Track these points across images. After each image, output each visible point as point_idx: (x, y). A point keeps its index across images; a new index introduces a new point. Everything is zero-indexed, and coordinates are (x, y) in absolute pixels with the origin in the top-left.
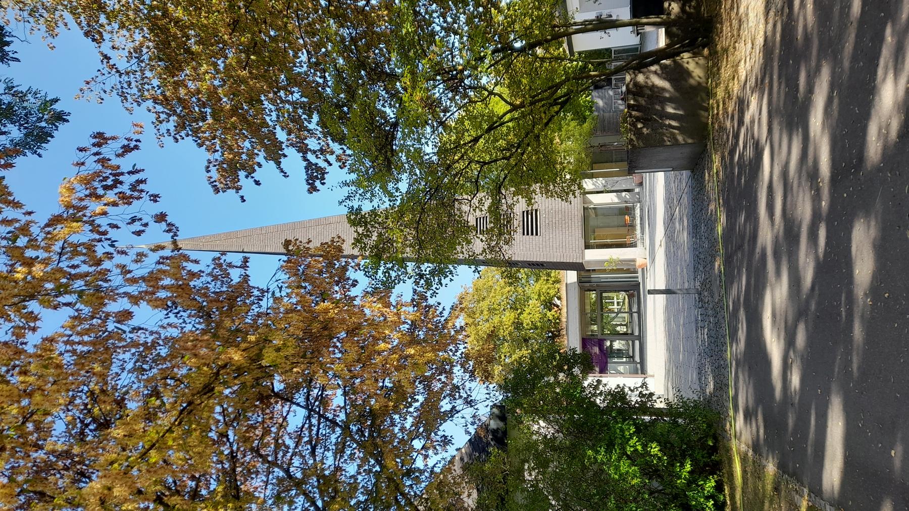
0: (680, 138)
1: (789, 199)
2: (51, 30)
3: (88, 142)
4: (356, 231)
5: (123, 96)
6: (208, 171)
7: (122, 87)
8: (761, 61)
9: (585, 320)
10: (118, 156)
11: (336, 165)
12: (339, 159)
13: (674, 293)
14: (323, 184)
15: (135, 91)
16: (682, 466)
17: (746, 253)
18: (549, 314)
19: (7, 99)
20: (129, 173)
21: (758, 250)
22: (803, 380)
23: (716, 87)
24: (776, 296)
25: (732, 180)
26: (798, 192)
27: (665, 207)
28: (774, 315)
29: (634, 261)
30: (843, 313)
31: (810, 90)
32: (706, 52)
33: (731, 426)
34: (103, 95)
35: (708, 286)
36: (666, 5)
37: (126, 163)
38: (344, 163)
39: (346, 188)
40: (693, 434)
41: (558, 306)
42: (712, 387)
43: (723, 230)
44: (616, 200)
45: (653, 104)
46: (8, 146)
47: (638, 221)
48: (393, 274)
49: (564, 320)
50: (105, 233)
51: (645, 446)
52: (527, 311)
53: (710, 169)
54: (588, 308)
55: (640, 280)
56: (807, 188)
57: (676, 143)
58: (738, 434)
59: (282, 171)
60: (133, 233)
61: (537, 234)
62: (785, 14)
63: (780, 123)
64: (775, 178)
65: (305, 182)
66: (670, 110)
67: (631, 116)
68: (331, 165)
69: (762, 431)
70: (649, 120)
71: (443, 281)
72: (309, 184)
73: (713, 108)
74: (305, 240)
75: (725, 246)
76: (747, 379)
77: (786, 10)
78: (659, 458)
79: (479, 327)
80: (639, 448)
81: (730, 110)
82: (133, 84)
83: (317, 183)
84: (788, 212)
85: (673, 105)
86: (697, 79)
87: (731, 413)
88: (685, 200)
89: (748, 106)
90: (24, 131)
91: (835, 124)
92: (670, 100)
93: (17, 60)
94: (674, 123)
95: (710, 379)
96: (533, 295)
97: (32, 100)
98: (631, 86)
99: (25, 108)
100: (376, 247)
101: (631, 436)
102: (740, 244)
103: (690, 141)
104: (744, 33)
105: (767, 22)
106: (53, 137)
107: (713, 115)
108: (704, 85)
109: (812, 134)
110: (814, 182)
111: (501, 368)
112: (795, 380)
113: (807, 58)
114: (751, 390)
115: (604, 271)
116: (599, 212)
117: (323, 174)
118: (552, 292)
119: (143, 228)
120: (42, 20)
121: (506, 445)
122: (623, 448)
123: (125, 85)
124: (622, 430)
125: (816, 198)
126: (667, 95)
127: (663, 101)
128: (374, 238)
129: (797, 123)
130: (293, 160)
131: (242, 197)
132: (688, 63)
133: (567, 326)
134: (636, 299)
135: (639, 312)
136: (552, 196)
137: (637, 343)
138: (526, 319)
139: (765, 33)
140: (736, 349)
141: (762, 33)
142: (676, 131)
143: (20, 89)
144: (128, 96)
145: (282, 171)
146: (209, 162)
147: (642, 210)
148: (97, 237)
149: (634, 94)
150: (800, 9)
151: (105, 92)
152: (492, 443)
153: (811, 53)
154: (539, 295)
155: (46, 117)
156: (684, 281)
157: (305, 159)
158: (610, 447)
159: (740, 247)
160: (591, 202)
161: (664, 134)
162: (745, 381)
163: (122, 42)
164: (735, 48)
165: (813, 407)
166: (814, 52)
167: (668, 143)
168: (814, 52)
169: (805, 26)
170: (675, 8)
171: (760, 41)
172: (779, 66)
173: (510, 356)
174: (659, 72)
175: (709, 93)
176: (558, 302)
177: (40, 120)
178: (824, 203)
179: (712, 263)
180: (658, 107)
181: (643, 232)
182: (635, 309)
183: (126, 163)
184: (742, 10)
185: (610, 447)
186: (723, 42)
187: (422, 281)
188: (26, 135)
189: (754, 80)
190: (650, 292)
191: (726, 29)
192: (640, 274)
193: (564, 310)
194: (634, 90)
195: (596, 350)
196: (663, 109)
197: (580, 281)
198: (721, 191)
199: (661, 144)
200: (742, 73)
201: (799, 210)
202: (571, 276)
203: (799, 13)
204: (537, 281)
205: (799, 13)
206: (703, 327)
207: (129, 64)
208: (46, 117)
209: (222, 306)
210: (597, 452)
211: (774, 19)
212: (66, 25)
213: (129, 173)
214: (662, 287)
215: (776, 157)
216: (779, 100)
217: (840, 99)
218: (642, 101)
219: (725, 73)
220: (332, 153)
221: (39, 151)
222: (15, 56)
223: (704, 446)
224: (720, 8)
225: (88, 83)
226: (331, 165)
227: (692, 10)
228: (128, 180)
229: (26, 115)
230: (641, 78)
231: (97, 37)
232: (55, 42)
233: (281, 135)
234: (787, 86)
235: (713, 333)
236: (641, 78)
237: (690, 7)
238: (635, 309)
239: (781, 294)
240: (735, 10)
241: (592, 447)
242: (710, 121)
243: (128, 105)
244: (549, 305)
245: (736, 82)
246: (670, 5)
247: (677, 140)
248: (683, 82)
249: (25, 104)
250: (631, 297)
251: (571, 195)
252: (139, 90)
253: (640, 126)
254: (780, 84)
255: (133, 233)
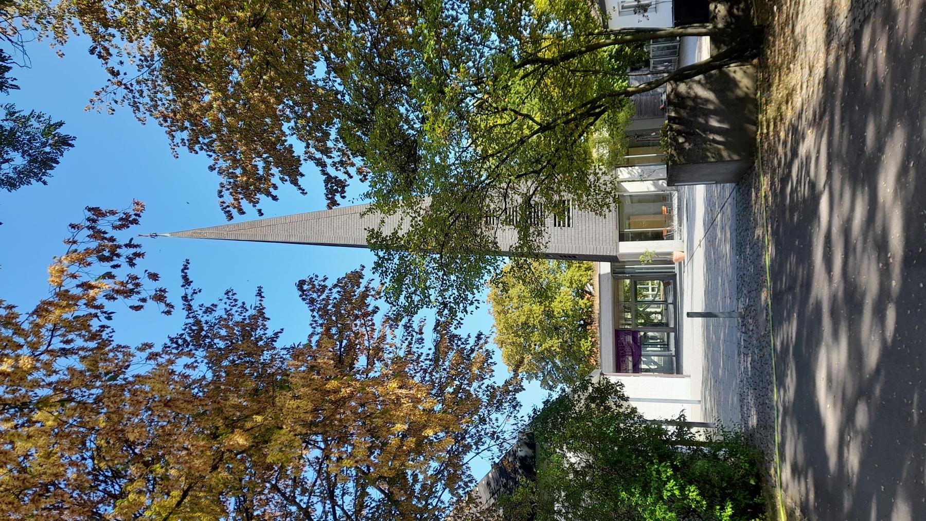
0: (725, 154)
1: (851, 259)
2: (60, 36)
3: (81, 217)
4: (377, 255)
5: (135, 106)
6: (221, 196)
7: (134, 97)
8: (821, 94)
9: (619, 308)
10: (115, 228)
11: (356, 177)
12: (359, 172)
13: (716, 316)
14: (344, 197)
15: (147, 100)
16: (723, 509)
17: (798, 298)
18: (581, 302)
19: (8, 125)
20: (126, 246)
21: (812, 300)
22: (863, 463)
23: (766, 104)
24: (831, 360)
25: (784, 212)
26: (862, 257)
27: (706, 208)
28: (829, 379)
29: (670, 254)
30: (915, 416)
31: (880, 148)
32: (755, 61)
33: (776, 472)
34: (114, 105)
35: (753, 314)
36: (712, 7)
37: (122, 237)
38: (365, 176)
39: (368, 201)
40: (731, 474)
41: (590, 293)
42: (755, 421)
43: (772, 261)
44: (652, 188)
45: (696, 116)
46: (11, 175)
47: (675, 212)
48: (416, 298)
49: (596, 307)
50: (100, 307)
51: (682, 489)
52: (559, 299)
53: (758, 190)
54: (622, 298)
55: (677, 271)
56: (874, 257)
57: (720, 159)
58: (784, 485)
59: (300, 189)
60: (131, 307)
61: (569, 226)
62: (850, 51)
63: (842, 172)
64: (835, 230)
65: (324, 197)
66: (714, 123)
67: (671, 129)
68: (351, 177)
69: (812, 496)
70: (692, 135)
71: (469, 309)
72: (328, 199)
73: (762, 126)
74: (321, 278)
75: (776, 276)
76: (796, 433)
77: (852, 48)
78: (698, 502)
79: (509, 315)
80: (677, 492)
81: (782, 134)
82: (145, 94)
83: (338, 197)
84: (850, 274)
85: (718, 118)
86: (745, 89)
87: (777, 458)
88: (728, 210)
89: (804, 138)
90: (27, 158)
91: (910, 199)
92: (715, 112)
93: (17, 87)
94: (718, 138)
95: (753, 412)
96: (564, 283)
97: (36, 125)
98: (672, 97)
99: (28, 133)
100: (398, 270)
101: (669, 479)
102: (792, 289)
103: (736, 157)
104: (801, 56)
105: (828, 53)
106: (57, 163)
107: (762, 133)
108: (752, 96)
109: (881, 199)
110: (883, 254)
111: (530, 357)
112: (853, 460)
113: (878, 113)
114: (800, 448)
115: (639, 262)
116: (635, 199)
117: (343, 187)
118: (584, 280)
119: (141, 304)
120: (50, 27)
121: (535, 474)
122: (660, 492)
123: (137, 95)
124: (658, 472)
125: (885, 273)
126: (711, 107)
127: (707, 114)
128: (396, 261)
129: (863, 180)
130: (311, 175)
131: (260, 211)
132: (735, 72)
133: (600, 318)
134: (671, 287)
135: (674, 303)
136: (585, 207)
137: (672, 335)
138: (556, 306)
139: (826, 64)
140: (783, 396)
141: (822, 62)
142: (721, 147)
143: (22, 114)
144: (141, 106)
145: (300, 189)
146: (222, 186)
147: (679, 199)
148: (93, 311)
149: (675, 105)
150: (869, 51)
151: (116, 102)
152: (520, 471)
153: (882, 107)
154: (571, 283)
155: (50, 142)
156: (725, 302)
157: (324, 172)
158: (645, 492)
159: (791, 288)
160: (626, 191)
161: (708, 150)
162: (793, 433)
163: (133, 53)
164: (789, 69)
165: (874, 497)
166: (886, 106)
167: (713, 160)
168: (886, 106)
169: (875, 74)
170: (721, 9)
171: (819, 71)
172: (842, 108)
173: (541, 345)
174: (703, 81)
175: (757, 107)
176: (591, 288)
177: (44, 145)
178: (894, 283)
179: (759, 292)
180: (701, 120)
181: (680, 224)
182: (670, 300)
183: (122, 237)
184: (798, 29)
185: (645, 492)
186: (775, 55)
187: (446, 311)
188: (29, 162)
189: (811, 112)
190: (689, 315)
191: (779, 43)
192: (676, 265)
193: (597, 302)
194: (676, 101)
195: (630, 339)
196: (707, 122)
197: (614, 272)
198: (771, 218)
199: (704, 159)
200: (798, 100)
201: (863, 278)
202: (605, 268)
203: (867, 56)
204: (569, 267)
205: (867, 56)
206: (746, 355)
207: (140, 73)
208: (50, 142)
209: (238, 341)
210: (633, 495)
211: (837, 52)
212: (75, 30)
213: (126, 246)
214: (700, 308)
215: (835, 207)
216: (841, 143)
217: (917, 172)
218: (684, 113)
219: (778, 93)
220: (353, 165)
221: (44, 178)
222: (14, 83)
223: (746, 485)
224: (773, 20)
225: (98, 94)
226: (351, 177)
227: (740, 13)
228: (126, 252)
229: (29, 141)
230: (682, 88)
231: (104, 53)
232: (64, 49)
233: (299, 148)
234: (851, 132)
235: (758, 366)
236: (682, 88)
237: (738, 10)
238: (670, 300)
239: (839, 359)
240: (790, 27)
241: (627, 490)
242: (758, 137)
243: (140, 115)
244: (581, 292)
245: (790, 108)
246: (716, 7)
247: (721, 156)
248: (729, 94)
249: (28, 129)
250: (666, 285)
251: (605, 208)
252: (152, 100)
253: (681, 140)
254: (842, 128)
255: (131, 307)
